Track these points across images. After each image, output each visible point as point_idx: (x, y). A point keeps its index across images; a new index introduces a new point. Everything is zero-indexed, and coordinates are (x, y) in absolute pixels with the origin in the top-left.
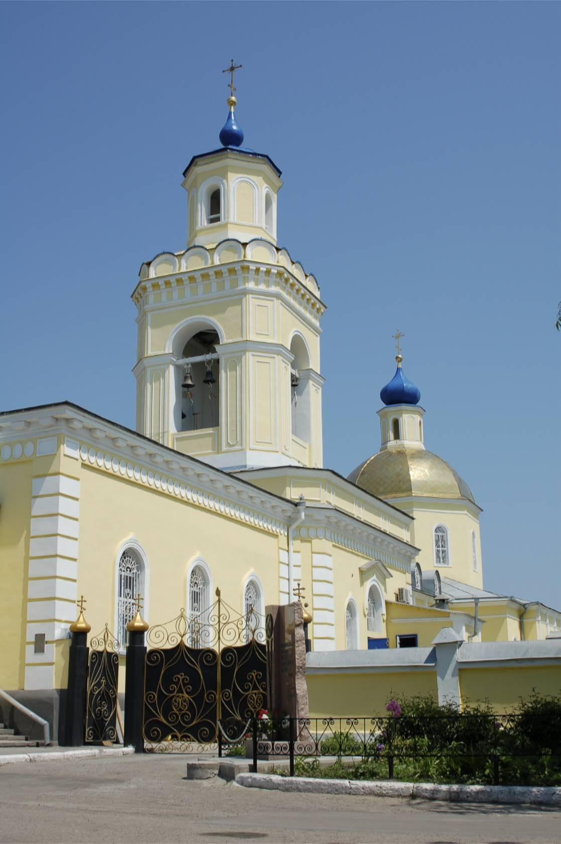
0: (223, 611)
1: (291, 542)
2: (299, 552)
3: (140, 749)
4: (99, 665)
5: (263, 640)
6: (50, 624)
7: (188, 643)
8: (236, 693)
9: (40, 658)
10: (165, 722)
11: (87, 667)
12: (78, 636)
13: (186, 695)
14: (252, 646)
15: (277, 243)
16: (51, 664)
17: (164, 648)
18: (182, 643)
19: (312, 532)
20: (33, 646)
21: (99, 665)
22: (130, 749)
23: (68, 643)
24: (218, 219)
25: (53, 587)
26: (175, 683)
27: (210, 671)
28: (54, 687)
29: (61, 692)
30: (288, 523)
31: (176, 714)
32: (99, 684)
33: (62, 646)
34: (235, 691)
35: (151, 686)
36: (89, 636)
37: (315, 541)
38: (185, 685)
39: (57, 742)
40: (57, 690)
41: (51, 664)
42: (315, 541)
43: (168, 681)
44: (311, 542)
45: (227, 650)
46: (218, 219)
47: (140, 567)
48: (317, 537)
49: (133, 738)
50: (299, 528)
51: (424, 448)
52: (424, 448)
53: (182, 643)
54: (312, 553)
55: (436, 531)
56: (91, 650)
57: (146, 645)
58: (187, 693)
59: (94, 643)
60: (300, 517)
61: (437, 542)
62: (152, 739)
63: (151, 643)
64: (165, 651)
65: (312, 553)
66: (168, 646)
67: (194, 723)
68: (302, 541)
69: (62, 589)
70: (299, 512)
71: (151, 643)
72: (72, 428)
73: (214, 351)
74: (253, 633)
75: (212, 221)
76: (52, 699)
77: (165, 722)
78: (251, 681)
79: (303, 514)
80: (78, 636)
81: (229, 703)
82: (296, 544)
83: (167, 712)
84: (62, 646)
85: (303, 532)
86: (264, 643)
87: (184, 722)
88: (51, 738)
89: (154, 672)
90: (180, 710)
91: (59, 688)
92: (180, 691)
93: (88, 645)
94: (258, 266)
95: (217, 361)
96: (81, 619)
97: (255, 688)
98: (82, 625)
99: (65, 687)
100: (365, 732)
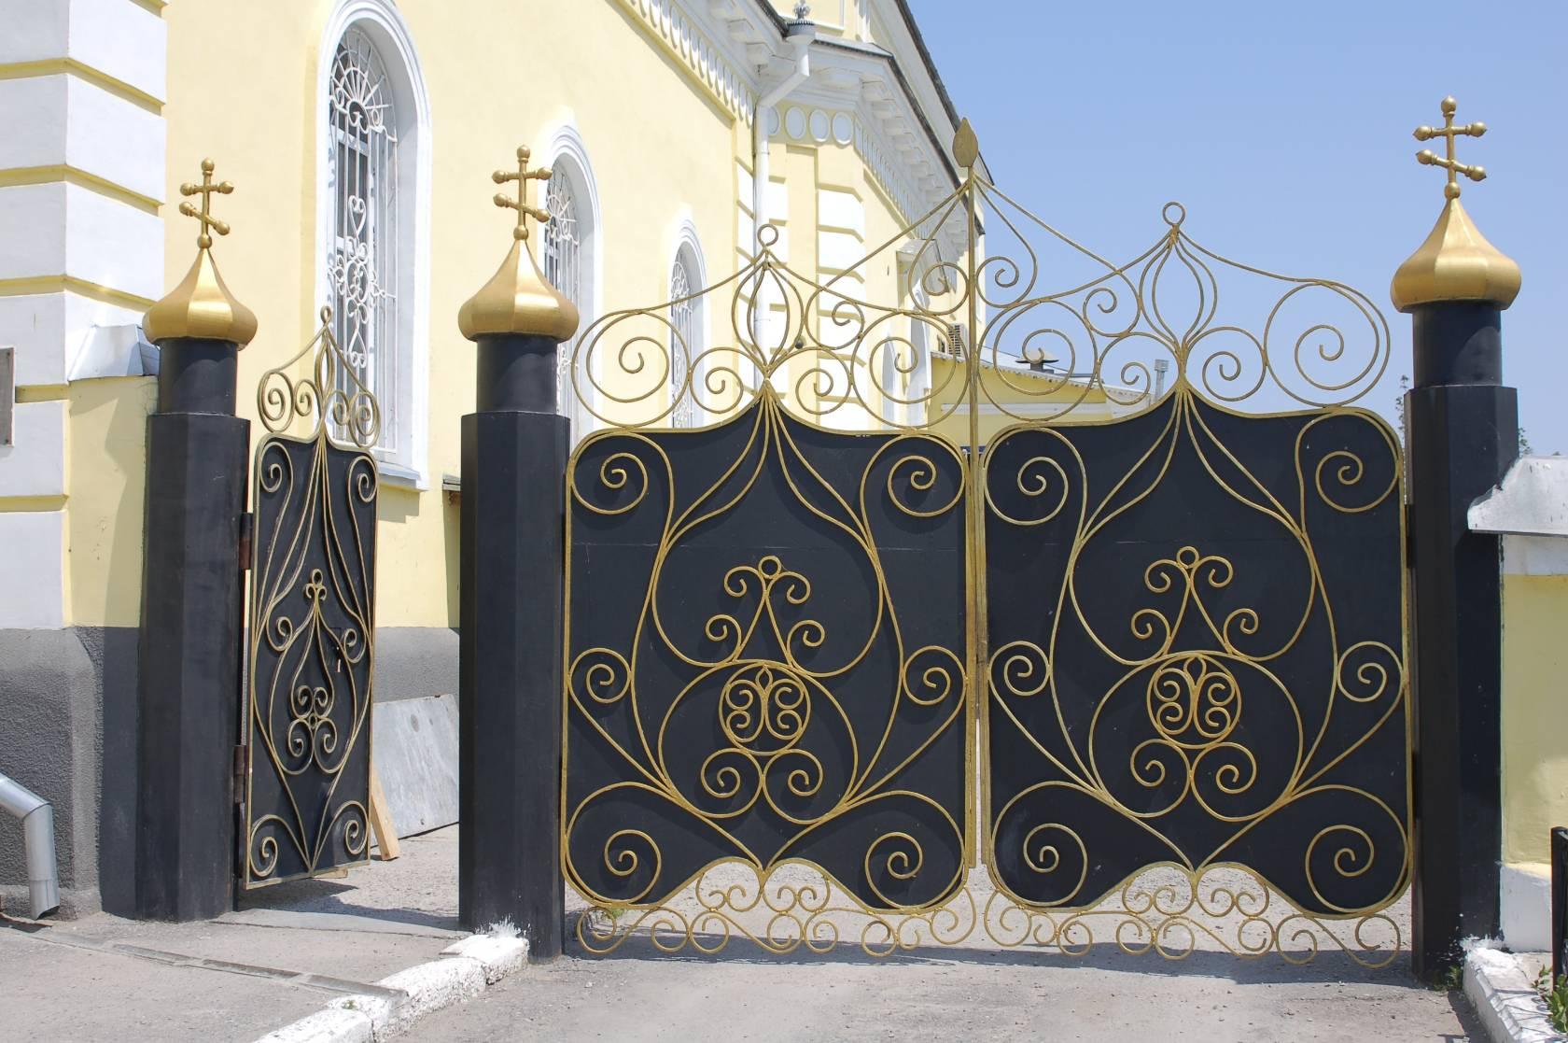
1: (763, 146)
2: (781, 180)
3: (553, 938)
4: (296, 509)
6: (37, 301)
8: (1083, 669)
11: (244, 521)
12: (192, 360)
13: (792, 667)
16: (52, 502)
17: (666, 425)
18: (765, 397)
19: (819, 122)
21: (296, 509)
22: (501, 946)
23: (144, 396)
25: (56, 118)
26: (730, 605)
28: (68, 617)
29: (107, 643)
30: (758, 84)
31: (739, 761)
32: (297, 604)
33: (110, 408)
34: (1073, 651)
35: (604, 616)
36: (250, 366)
37: (826, 152)
38: (788, 614)
39: (92, 893)
40: (85, 632)
41: (52, 502)
42: (826, 152)
43: (694, 588)
44: (814, 152)
45: (1018, 448)
47: (400, 112)
48: (832, 140)
49: (499, 875)
50: (781, 110)
51: (115, 401)
52: (115, 401)
53: (765, 397)
54: (819, 186)
56: (258, 435)
57: (564, 404)
58: (804, 656)
59: (272, 391)
60: (796, 69)
62: (610, 886)
63: (610, 392)
65: (819, 186)
67: (842, 807)
68: (792, 148)
69: (93, 131)
70: (792, 57)
74: (1182, 353)
76: (57, 680)
78: (1169, 603)
79: (806, 59)
80: (192, 360)
81: (1037, 711)
82: (774, 157)
83: (693, 745)
84: (110, 408)
85: (795, 119)
88: (65, 877)
89: (615, 544)
90: (766, 742)
91: (100, 622)
93: (245, 407)
96: (206, 279)
97: (1193, 635)
98: (209, 307)
99: (130, 617)
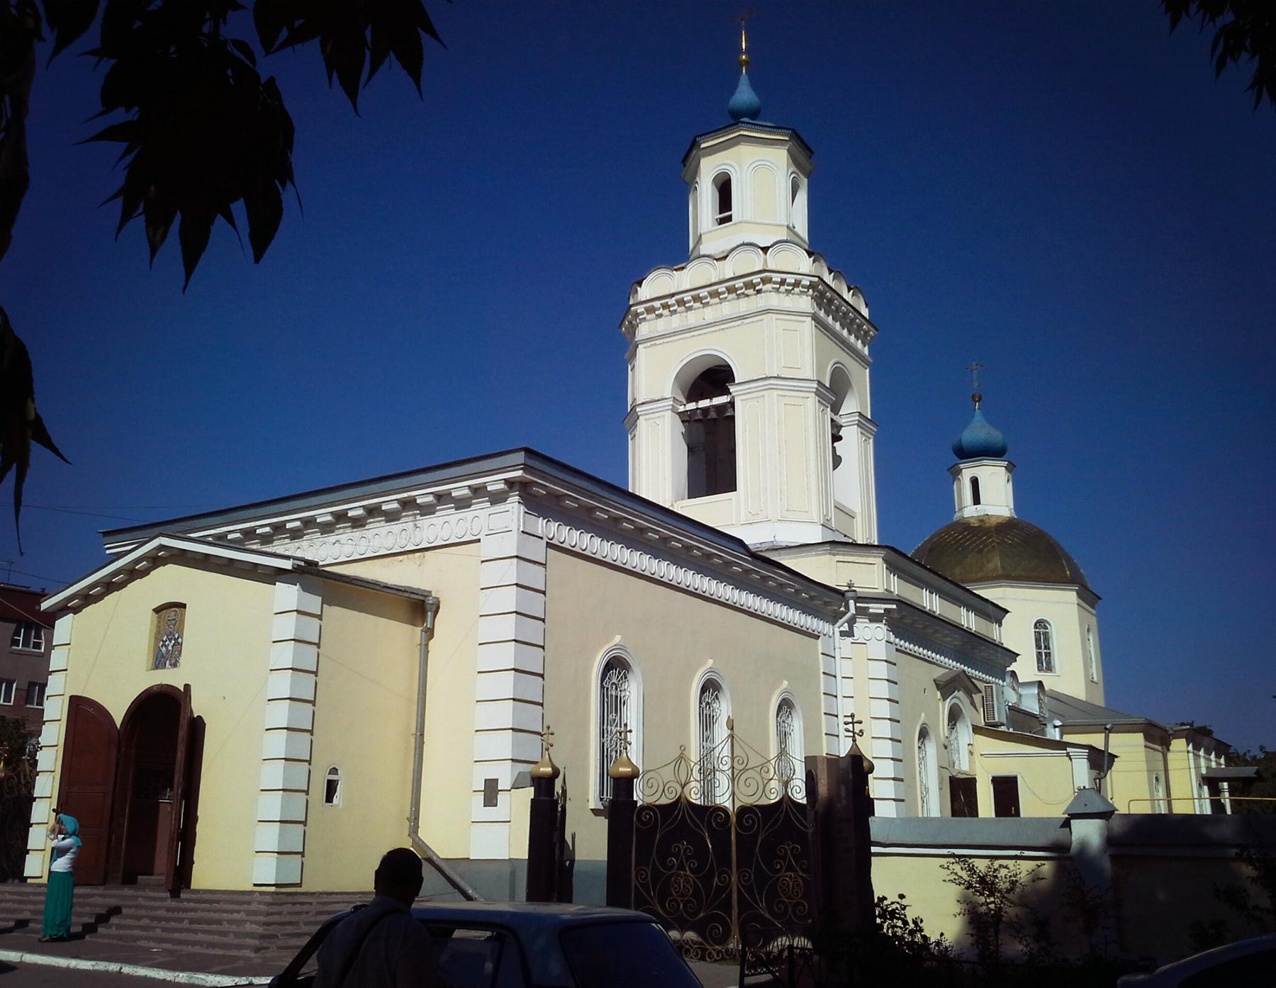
0: (737, 751)
5: (800, 796)
7: (696, 798)
9: (491, 813)
10: (767, 916)
14: (786, 802)
15: (810, 245)
20: (481, 796)
24: (729, 219)
27: (721, 834)
45: (744, 811)
46: (729, 219)
55: (1036, 627)
61: (1038, 641)
64: (661, 807)
66: (664, 801)
71: (639, 796)
72: (530, 495)
73: (728, 393)
75: (722, 221)
77: (767, 916)
83: (664, 895)
86: (804, 801)
87: (686, 912)
92: (682, 867)
94: (784, 276)
95: (732, 404)
97: (790, 868)
100: (31, 925)
